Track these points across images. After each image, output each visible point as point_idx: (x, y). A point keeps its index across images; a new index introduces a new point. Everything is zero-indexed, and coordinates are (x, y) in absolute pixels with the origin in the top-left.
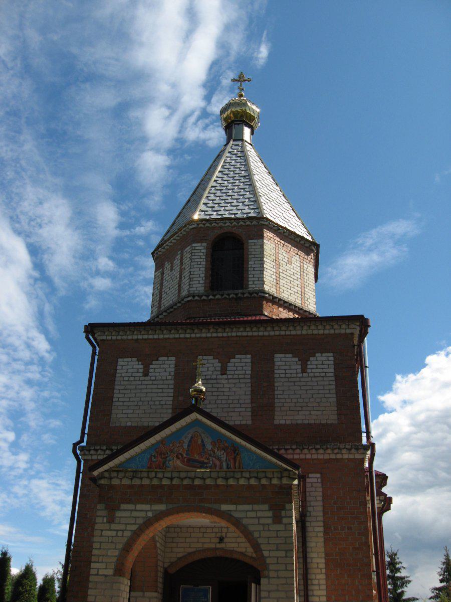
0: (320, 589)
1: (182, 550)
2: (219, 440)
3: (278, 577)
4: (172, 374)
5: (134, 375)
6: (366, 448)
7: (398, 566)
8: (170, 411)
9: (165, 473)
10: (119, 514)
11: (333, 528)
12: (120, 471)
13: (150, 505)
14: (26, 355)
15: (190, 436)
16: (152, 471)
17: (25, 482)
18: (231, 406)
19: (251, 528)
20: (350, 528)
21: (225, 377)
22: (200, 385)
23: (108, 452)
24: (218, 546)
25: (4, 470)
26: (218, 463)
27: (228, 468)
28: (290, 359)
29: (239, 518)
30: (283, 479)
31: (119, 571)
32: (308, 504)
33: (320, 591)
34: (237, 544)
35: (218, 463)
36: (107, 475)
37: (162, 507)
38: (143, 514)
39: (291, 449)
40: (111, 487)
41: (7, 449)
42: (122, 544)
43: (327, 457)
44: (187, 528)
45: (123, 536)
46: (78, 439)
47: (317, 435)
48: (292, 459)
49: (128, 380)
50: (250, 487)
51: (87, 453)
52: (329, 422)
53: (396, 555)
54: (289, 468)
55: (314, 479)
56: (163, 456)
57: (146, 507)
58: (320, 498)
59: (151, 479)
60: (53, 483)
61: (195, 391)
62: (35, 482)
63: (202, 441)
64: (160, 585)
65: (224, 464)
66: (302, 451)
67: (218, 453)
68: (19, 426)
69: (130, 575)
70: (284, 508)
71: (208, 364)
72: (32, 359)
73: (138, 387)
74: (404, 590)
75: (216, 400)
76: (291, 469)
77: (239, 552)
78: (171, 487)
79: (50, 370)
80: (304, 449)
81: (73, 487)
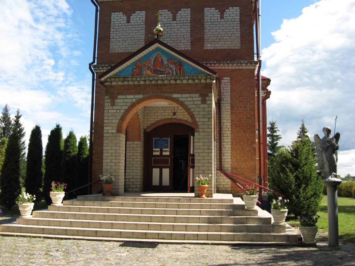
0: (227, 139)
1: (153, 120)
2: (171, 59)
3: (204, 132)
4: (144, 21)
5: (121, 22)
6: (256, 63)
7: (275, 130)
8: (144, 43)
9: (141, 78)
10: (117, 101)
11: (236, 107)
12: (117, 77)
13: (134, 96)
14: (55, 12)
15: (154, 57)
16: (134, 77)
17: (64, 88)
18: (179, 39)
19: (189, 107)
20: (245, 107)
21: (175, 22)
22: (159, 27)
23: (109, 68)
24: (173, 117)
25: (51, 82)
26: (171, 71)
27: (176, 74)
28: (214, 11)
29: (183, 101)
30: (207, 80)
31: (119, 131)
32: (222, 94)
33: (228, 140)
34: (183, 116)
35: (171, 71)
36: (109, 80)
37: (141, 96)
38: (130, 100)
39: (214, 63)
40: (112, 86)
41: (51, 70)
42: (119, 117)
43: (234, 68)
44: (156, 108)
45: (120, 112)
46: (92, 61)
47: (228, 56)
48: (213, 69)
49: (118, 26)
50: (189, 84)
51: (97, 69)
52: (236, 48)
53: (274, 123)
54: (210, 74)
55: (226, 80)
56: (140, 69)
57: (132, 97)
58: (229, 91)
59: (134, 81)
60: (80, 88)
61: (157, 31)
62: (70, 88)
63: (162, 59)
64: (142, 138)
65: (174, 72)
66: (219, 64)
67: (171, 66)
68: (56, 56)
69: (125, 133)
70: (207, 96)
71: (164, 15)
72: (59, 15)
73: (124, 29)
74: (277, 142)
75: (170, 36)
76: (212, 74)
77: (184, 120)
78: (145, 85)
79: (71, 21)
80: (220, 63)
81: (91, 90)
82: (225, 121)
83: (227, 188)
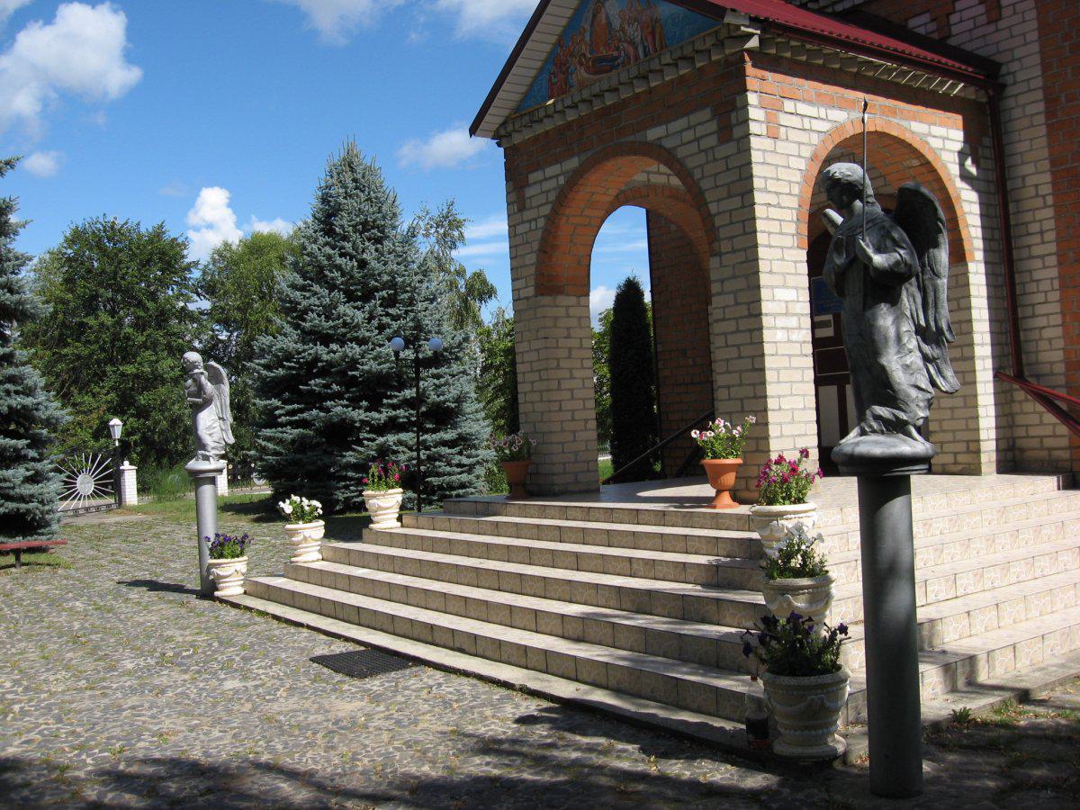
11: (1063, 99)
37: (574, 163)
57: (553, 170)
58: (1034, 36)
82: (1029, 169)
83: (1056, 449)
